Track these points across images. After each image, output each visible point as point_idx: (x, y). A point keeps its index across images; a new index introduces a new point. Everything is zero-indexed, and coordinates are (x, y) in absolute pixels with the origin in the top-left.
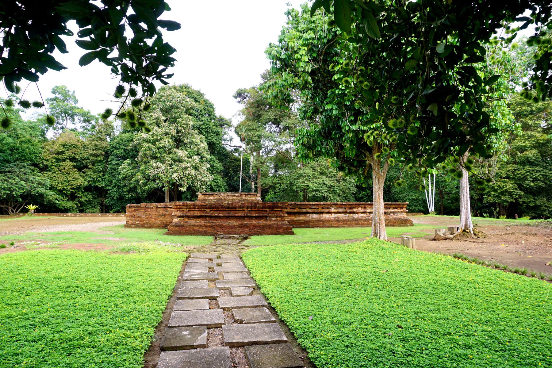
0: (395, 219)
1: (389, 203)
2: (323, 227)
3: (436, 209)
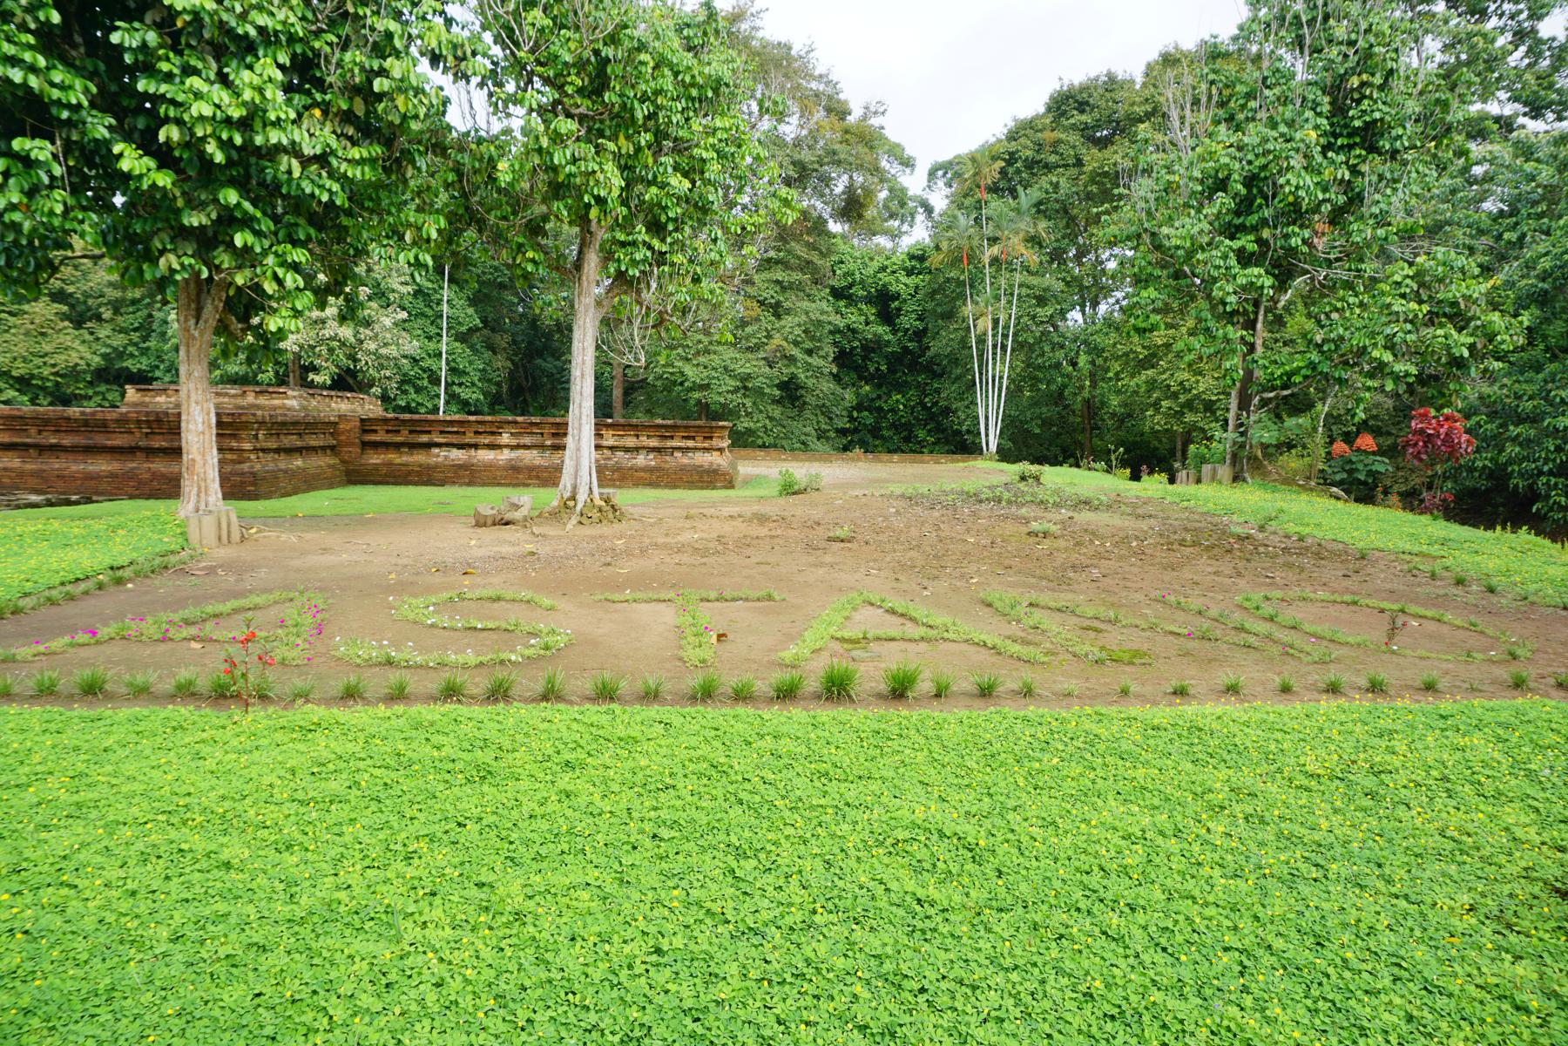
0: (683, 469)
1: (669, 422)
2: (470, 484)
3: (1000, 450)
